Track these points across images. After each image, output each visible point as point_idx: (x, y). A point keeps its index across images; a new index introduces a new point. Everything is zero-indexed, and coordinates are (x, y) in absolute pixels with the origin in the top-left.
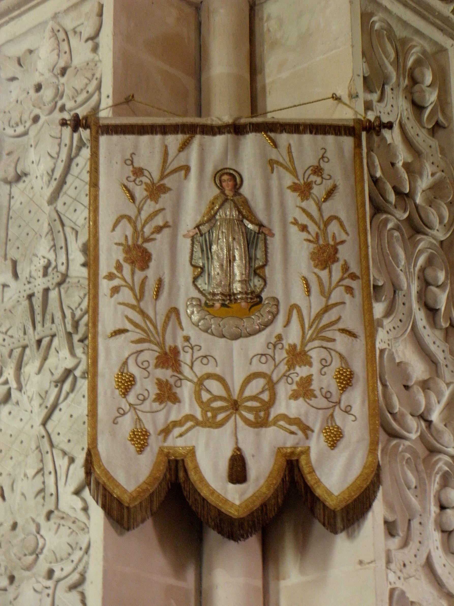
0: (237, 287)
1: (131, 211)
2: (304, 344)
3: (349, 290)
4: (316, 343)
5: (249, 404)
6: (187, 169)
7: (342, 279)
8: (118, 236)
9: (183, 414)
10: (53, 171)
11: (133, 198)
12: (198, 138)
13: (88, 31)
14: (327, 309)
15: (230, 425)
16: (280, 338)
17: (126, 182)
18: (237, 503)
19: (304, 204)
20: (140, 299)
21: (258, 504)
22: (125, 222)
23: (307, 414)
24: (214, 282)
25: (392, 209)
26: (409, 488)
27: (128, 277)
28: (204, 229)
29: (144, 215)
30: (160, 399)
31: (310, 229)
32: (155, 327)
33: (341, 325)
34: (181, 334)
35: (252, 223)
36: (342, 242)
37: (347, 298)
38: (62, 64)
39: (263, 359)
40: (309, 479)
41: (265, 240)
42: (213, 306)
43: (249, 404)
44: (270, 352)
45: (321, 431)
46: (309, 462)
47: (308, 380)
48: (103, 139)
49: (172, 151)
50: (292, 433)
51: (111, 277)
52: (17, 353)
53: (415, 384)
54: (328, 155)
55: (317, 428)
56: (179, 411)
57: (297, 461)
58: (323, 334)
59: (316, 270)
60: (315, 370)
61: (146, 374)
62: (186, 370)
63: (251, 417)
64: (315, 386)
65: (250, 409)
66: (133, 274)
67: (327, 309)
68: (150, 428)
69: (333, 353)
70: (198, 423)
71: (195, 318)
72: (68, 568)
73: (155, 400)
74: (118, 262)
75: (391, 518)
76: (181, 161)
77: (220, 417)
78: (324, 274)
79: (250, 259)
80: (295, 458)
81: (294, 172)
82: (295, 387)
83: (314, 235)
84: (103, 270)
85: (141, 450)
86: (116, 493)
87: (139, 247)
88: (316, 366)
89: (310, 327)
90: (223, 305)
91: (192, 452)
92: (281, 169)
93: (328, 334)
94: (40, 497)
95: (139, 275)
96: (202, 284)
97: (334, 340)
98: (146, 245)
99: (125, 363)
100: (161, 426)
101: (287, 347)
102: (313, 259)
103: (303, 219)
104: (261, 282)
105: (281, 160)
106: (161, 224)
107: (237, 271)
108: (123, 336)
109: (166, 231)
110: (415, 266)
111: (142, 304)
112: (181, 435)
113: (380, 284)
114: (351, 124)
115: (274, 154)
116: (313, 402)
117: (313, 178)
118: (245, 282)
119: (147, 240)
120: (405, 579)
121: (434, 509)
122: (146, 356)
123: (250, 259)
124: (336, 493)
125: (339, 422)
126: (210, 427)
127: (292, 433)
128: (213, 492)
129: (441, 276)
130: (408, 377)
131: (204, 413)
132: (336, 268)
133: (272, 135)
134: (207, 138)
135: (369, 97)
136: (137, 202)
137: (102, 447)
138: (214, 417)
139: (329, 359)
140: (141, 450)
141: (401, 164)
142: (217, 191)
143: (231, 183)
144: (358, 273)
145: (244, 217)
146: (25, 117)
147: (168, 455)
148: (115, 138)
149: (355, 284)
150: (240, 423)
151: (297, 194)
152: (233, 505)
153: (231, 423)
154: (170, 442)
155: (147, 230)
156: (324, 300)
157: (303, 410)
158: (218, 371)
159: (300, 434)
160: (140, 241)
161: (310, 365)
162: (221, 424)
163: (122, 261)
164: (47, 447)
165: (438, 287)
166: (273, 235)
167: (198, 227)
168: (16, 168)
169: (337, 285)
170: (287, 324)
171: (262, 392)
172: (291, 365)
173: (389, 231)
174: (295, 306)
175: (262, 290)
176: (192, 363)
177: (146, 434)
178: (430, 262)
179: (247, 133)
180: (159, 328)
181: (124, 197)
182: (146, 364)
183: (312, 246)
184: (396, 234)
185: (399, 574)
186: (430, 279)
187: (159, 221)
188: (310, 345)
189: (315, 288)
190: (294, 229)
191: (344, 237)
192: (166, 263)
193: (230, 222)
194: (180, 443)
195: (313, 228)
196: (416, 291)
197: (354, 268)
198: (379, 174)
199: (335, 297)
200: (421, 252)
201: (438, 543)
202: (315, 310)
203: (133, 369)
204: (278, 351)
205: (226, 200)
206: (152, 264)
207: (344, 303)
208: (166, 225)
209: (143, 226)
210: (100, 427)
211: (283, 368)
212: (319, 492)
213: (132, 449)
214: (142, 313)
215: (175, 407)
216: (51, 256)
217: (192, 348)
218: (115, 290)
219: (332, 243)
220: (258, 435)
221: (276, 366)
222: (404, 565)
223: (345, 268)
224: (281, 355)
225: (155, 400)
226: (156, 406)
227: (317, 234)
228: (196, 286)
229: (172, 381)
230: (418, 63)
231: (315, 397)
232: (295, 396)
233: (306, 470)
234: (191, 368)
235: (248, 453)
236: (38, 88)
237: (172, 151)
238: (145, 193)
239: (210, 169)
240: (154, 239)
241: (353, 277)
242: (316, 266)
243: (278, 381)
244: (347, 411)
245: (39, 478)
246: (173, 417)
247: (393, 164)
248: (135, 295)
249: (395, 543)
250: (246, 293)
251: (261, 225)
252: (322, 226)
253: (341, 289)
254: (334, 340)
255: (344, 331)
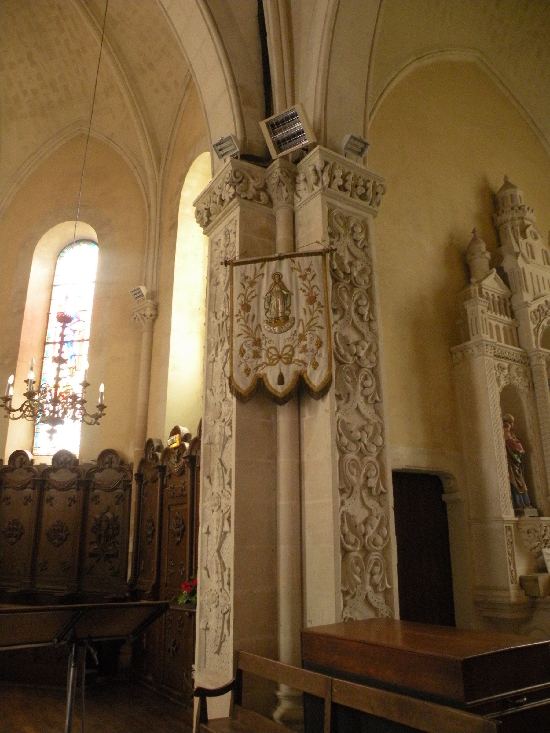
0: (280, 315)
1: (244, 292)
2: (304, 333)
3: (321, 312)
4: (308, 332)
5: (285, 356)
6: (263, 274)
7: (318, 308)
8: (239, 301)
9: (262, 362)
10: (225, 280)
11: (244, 287)
12: (267, 263)
13: (233, 231)
14: (312, 319)
15: (278, 365)
16: (295, 331)
17: (242, 282)
18: (281, 392)
19: (304, 282)
20: (246, 323)
21: (288, 392)
22: (242, 296)
23: (305, 358)
24: (272, 314)
25: (341, 280)
26: (348, 382)
27: (243, 315)
28: (269, 295)
29: (248, 292)
30: (254, 357)
31: (306, 291)
32: (252, 332)
33: (317, 325)
34: (261, 333)
35: (285, 291)
36: (318, 295)
37: (320, 314)
38: (227, 243)
39: (290, 340)
40: (307, 382)
41: (290, 297)
42: (272, 322)
43: (285, 356)
44: (292, 337)
45: (310, 364)
46: (307, 375)
47: (305, 346)
48: (235, 268)
49: (258, 268)
50: (300, 365)
51: (237, 316)
52: (216, 345)
53: (352, 343)
54: (313, 263)
55: (309, 364)
56: (261, 361)
57: (303, 375)
58: (311, 329)
59: (308, 306)
60: (308, 342)
61: (249, 349)
62: (263, 346)
63: (285, 361)
64: (308, 348)
65: (285, 358)
66: (244, 314)
67: (312, 319)
68: (251, 367)
69: (315, 336)
70: (267, 365)
71: (266, 327)
72: (228, 418)
73: (252, 358)
74: (239, 310)
75: (338, 393)
76: (261, 272)
77: (275, 362)
78: (311, 307)
79: (284, 304)
80: (302, 374)
81: (300, 271)
82: (301, 349)
83: (308, 293)
84: (235, 314)
85: (248, 375)
86: (240, 391)
87: (247, 304)
88: (308, 340)
89: (306, 326)
90: (275, 322)
91: (265, 375)
92: (296, 270)
93: (313, 328)
94: (221, 394)
95: (247, 314)
96: (268, 315)
97: (315, 331)
98: (248, 303)
99: (242, 346)
100: (255, 367)
101: (298, 334)
102: (307, 302)
103: (304, 288)
104: (289, 312)
105: (296, 267)
106: (254, 295)
107: (280, 309)
108: (241, 336)
109: (256, 298)
110: (353, 300)
111: (248, 325)
112: (262, 369)
113: (335, 308)
114: (321, 251)
115: (293, 265)
116: (307, 354)
117: (307, 272)
118: (283, 313)
119: (249, 301)
120: (346, 415)
121: (360, 388)
122: (249, 342)
123: (284, 304)
124: (317, 386)
125: (317, 361)
126: (271, 365)
127: (300, 365)
128: (273, 389)
129: (365, 302)
130: (348, 341)
131: (269, 360)
132: (316, 305)
133: (293, 259)
134: (270, 263)
135: (333, 240)
136: (246, 288)
137: (234, 376)
138: (273, 362)
139: (313, 337)
140: (248, 375)
141: (347, 263)
142: (273, 281)
143: (278, 278)
144: (324, 305)
145: (282, 289)
146: (218, 263)
147: (257, 377)
148: (238, 267)
149: (322, 309)
150: (282, 363)
151: (301, 279)
152: (279, 393)
153: (278, 364)
154: (258, 372)
155: (249, 298)
156: (311, 316)
157: (304, 357)
158: (274, 345)
159: (303, 366)
160: (247, 302)
161: (306, 340)
162: (275, 365)
163: (241, 310)
164: (223, 376)
165: (364, 306)
166: (293, 295)
167: (266, 295)
168: (216, 281)
169: (316, 310)
170: (298, 326)
171: (290, 351)
172: (300, 341)
173: (340, 288)
174: (301, 320)
175: (289, 315)
176: (265, 343)
177: (249, 370)
178: (360, 298)
179: (284, 259)
180: (254, 332)
181: (241, 286)
182: (249, 345)
183: (307, 297)
184: (343, 289)
185: (343, 413)
186: (360, 304)
187: (253, 294)
188: (306, 333)
189: (308, 312)
190: (301, 292)
191: (318, 292)
192: (256, 308)
193: (277, 292)
194: (262, 372)
195: (307, 290)
196: (354, 309)
197: (322, 303)
198: (335, 267)
199: (315, 316)
200: (355, 295)
201: (363, 401)
202: (308, 320)
203: (245, 347)
204: (295, 337)
205: (275, 284)
206: (251, 310)
207: (318, 317)
208: (256, 295)
209: (248, 296)
210: (234, 368)
211: (297, 342)
212: (311, 386)
213: (245, 375)
214: (248, 327)
215: (260, 359)
216: (224, 310)
217: (265, 338)
218: (239, 320)
219: (314, 295)
220: (288, 367)
221: (294, 342)
222: (346, 410)
223: (319, 304)
224: (296, 338)
225: (252, 358)
226: (253, 360)
227: (309, 293)
228: (266, 316)
229: (258, 350)
230: (355, 225)
231: (308, 352)
232: (301, 352)
233: (306, 378)
234: (265, 345)
235: (284, 373)
236: (222, 252)
237: (258, 268)
238: (249, 285)
239: (271, 273)
240: (251, 301)
241: (322, 307)
242: (308, 304)
243: (295, 347)
244: (320, 356)
245: (221, 387)
246: (259, 363)
247: (343, 264)
248: (245, 322)
249: (342, 403)
250: (283, 317)
251: (288, 291)
252: (310, 289)
253: (318, 312)
254: (315, 331)
255: (319, 327)
